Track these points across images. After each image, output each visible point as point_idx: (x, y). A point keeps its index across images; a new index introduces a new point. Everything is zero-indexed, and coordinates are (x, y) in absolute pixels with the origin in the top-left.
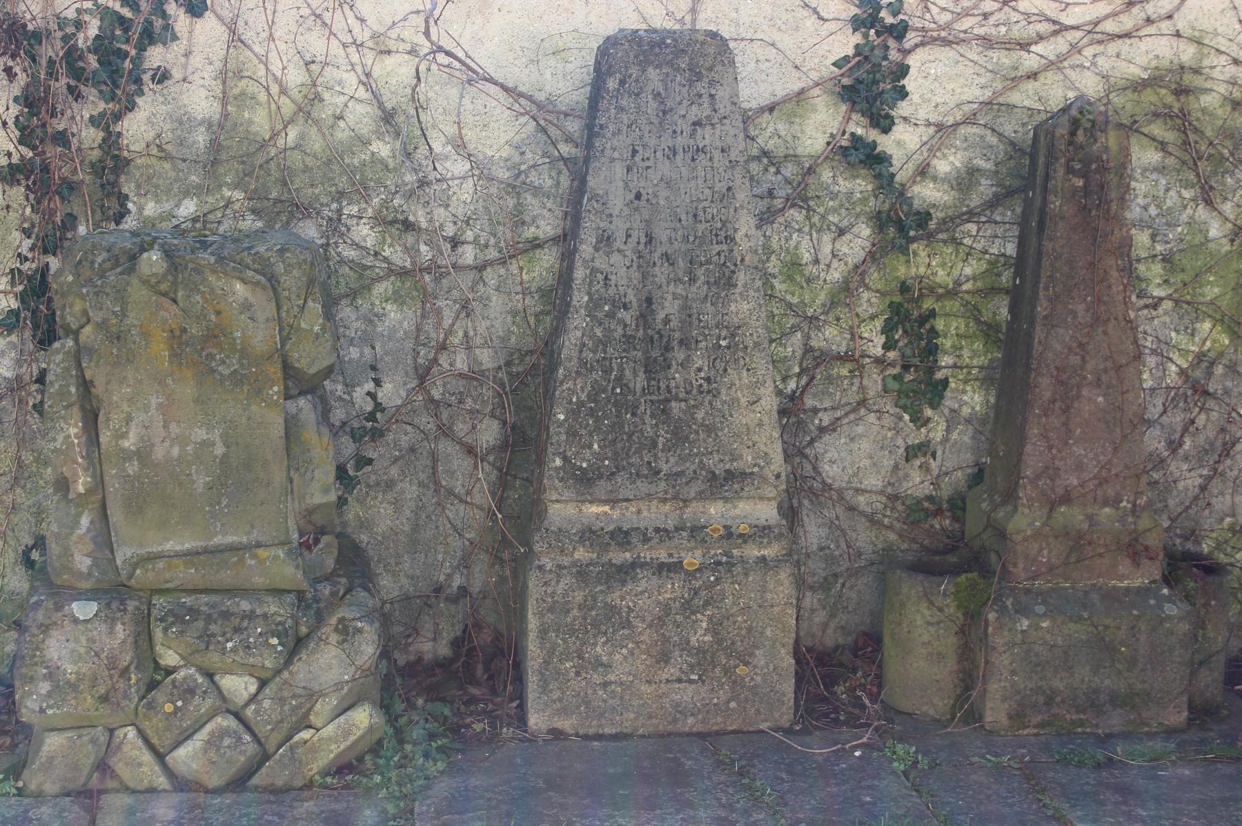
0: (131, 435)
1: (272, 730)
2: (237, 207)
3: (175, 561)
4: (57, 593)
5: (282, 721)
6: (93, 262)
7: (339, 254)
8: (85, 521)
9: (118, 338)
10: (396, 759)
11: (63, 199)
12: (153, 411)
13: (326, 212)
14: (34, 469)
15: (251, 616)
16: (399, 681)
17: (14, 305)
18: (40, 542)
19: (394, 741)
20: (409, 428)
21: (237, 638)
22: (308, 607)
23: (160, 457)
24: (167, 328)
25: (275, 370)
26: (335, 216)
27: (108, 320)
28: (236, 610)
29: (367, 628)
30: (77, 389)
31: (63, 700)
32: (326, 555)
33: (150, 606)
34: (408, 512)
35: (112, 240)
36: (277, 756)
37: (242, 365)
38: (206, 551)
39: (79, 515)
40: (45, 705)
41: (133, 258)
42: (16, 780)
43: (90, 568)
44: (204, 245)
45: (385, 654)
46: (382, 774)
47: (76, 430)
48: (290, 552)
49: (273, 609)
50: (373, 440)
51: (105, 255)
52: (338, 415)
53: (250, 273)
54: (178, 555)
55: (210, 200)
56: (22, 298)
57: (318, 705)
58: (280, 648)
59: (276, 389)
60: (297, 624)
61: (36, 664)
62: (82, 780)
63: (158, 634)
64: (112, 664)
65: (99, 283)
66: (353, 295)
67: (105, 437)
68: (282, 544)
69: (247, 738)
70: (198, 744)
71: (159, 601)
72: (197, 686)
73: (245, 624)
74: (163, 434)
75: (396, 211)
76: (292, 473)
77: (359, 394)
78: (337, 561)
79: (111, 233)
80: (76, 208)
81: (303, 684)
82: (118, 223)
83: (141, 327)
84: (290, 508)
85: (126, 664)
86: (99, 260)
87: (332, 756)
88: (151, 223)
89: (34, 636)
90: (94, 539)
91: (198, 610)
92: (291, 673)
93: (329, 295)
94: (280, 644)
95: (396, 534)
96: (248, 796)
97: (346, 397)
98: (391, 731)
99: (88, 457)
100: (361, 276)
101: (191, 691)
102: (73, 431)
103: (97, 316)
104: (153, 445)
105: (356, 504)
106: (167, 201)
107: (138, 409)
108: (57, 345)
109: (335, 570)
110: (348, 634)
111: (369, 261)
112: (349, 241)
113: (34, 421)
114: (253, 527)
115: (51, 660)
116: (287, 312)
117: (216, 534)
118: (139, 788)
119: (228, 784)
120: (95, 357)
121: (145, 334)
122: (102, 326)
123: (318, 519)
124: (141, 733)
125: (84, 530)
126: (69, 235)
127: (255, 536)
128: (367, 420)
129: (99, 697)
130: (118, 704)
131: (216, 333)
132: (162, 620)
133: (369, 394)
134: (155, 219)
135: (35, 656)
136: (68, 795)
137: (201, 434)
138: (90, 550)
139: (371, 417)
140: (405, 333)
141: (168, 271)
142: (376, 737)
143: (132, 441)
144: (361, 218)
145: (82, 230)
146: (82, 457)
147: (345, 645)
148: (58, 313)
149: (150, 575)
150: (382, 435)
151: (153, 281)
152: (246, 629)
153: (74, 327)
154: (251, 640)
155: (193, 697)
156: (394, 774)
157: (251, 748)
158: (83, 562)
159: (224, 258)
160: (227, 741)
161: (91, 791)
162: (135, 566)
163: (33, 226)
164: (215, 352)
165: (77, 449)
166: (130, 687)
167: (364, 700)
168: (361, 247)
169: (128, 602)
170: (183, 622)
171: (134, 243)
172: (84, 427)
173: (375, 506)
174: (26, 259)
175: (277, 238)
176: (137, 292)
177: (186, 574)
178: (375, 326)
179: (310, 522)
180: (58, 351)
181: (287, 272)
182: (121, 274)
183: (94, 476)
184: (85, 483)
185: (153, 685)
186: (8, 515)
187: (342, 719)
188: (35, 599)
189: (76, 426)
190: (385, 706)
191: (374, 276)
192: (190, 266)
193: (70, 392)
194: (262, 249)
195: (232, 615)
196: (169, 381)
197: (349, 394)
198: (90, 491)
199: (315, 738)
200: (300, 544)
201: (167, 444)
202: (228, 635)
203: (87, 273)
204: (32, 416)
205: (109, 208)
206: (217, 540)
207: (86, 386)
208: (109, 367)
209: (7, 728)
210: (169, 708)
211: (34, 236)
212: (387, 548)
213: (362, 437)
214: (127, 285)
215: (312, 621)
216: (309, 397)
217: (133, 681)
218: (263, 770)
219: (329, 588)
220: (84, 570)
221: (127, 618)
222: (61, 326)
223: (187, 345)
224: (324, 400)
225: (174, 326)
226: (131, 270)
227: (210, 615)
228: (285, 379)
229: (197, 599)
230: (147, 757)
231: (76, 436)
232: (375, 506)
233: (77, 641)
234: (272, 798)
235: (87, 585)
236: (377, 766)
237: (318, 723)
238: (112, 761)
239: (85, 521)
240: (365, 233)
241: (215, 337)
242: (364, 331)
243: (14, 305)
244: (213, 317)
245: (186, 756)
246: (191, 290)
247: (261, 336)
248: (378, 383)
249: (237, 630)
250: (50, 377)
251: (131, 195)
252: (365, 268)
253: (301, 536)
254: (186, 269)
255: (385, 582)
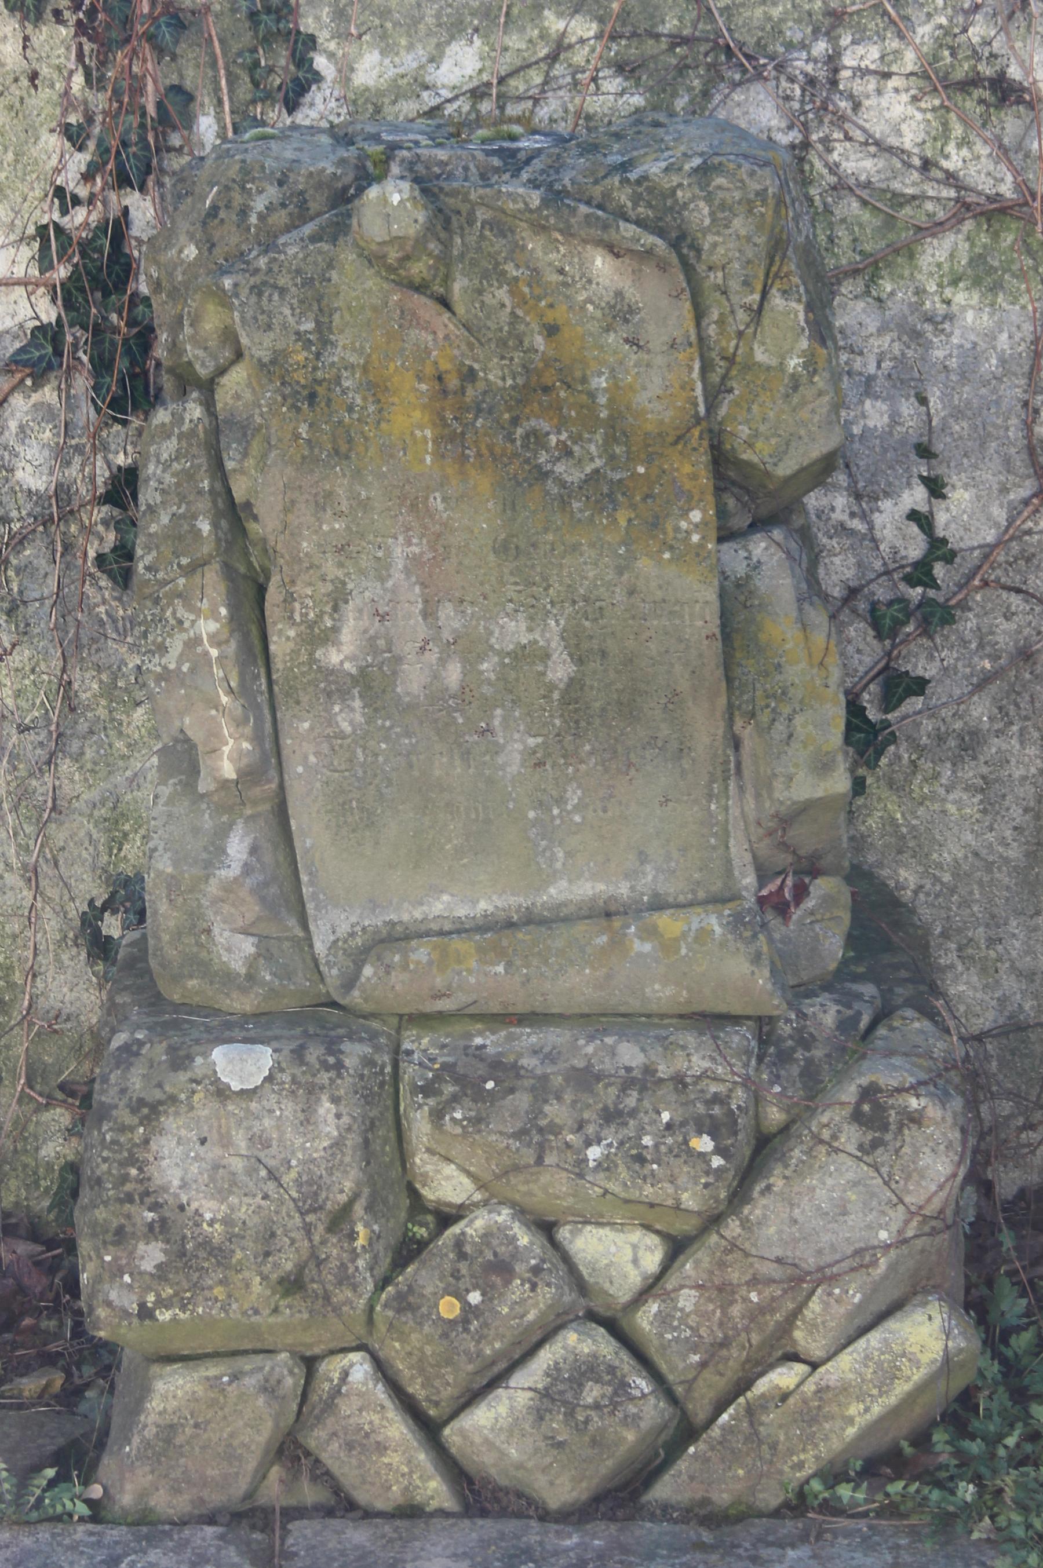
0: (346, 635)
1: (703, 1365)
2: (579, 57)
3: (457, 944)
4: (175, 1025)
5: (725, 1344)
6: (244, 212)
7: (833, 168)
8: (237, 847)
9: (312, 397)
10: (1011, 1441)
11: (160, 51)
12: (397, 575)
13: (800, 64)
14: (102, 712)
15: (644, 1081)
16: (1007, 1240)
17: (48, 312)
18: (127, 895)
19: (1002, 1396)
20: (1015, 601)
21: (610, 1137)
22: (784, 1057)
23: (415, 688)
24: (429, 370)
25: (692, 468)
26: (822, 74)
27: (285, 354)
28: (608, 1066)
29: (934, 1112)
30: (215, 525)
31: (195, 1286)
32: (824, 924)
33: (397, 1053)
34: (1016, 812)
35: (289, 154)
36: (715, 1432)
37: (612, 458)
38: (531, 919)
39: (223, 833)
40: (151, 1298)
41: (343, 198)
42: (86, 1483)
43: (252, 963)
44: (513, 162)
45: (978, 1180)
46: (977, 1479)
47: (213, 626)
48: (737, 922)
49: (699, 1063)
50: (926, 630)
51: (273, 192)
52: (839, 569)
53: (628, 230)
54: (461, 929)
55: (515, 41)
56: (69, 296)
57: (815, 1305)
58: (717, 1162)
59: (696, 516)
60: (757, 1099)
61: (129, 1198)
62: (242, 1486)
63: (420, 1126)
64: (310, 1201)
65: (262, 262)
66: (870, 269)
67: (282, 642)
68: (716, 900)
69: (642, 1384)
70: (523, 1398)
71: (419, 1043)
72: (516, 1254)
73: (631, 1100)
74: (422, 631)
75: (976, 55)
76: (739, 723)
77: (889, 517)
78: (851, 940)
79: (283, 136)
80: (190, 72)
81: (778, 1252)
82: (292, 107)
83: (365, 369)
84: (734, 812)
85: (343, 1198)
86: (259, 204)
87: (851, 1431)
88: (369, 104)
89: (123, 1129)
90: (257, 891)
91: (515, 1067)
92: (745, 1223)
93: (819, 277)
94: (718, 1151)
95: (989, 867)
96: (647, 1530)
97: (857, 524)
98: (994, 1369)
99: (244, 692)
100: (890, 221)
101: (501, 1269)
102: (207, 627)
103: (258, 345)
104: (398, 660)
105: (885, 793)
106: (410, 47)
107: (362, 572)
108: (162, 416)
109: (845, 962)
110: (885, 1127)
111: (908, 184)
112: (858, 135)
113: (101, 594)
114: (643, 857)
115: (165, 1189)
116: (721, 322)
117: (552, 877)
118: (380, 1505)
119: (597, 1499)
120: (256, 447)
121: (377, 389)
122: (272, 368)
123: (806, 837)
124: (382, 1368)
125: (234, 870)
126: (175, 140)
127: (649, 880)
128: (911, 581)
129: (281, 1281)
130: (327, 1297)
131: (548, 379)
132: (428, 1090)
133: (914, 516)
134: (380, 93)
135: (125, 1178)
136: (211, 1520)
137: (513, 631)
138: (250, 917)
139: (921, 573)
140: (1003, 361)
141: (429, 228)
142: (959, 1383)
143: (348, 649)
144: (887, 75)
145: (206, 126)
146: (231, 691)
147: (881, 1155)
148: (164, 337)
149: (398, 979)
150: (948, 618)
151: (393, 255)
152: (633, 1113)
153: (203, 372)
154: (647, 1141)
155: (507, 1283)
156: (1008, 1480)
157: (651, 1411)
158: (235, 950)
159: (563, 194)
160: (592, 1393)
161: (267, 1512)
162: (360, 957)
163: (90, 119)
164: (545, 426)
165: (218, 673)
166: (354, 1255)
167: (925, 1291)
168: (890, 150)
169: (347, 1046)
170: (480, 1095)
171: (342, 162)
172: (232, 618)
173: (933, 797)
174: (76, 201)
175: (691, 142)
176: (355, 285)
177: (481, 977)
178: (928, 346)
179: (784, 846)
180: (165, 432)
181: (720, 223)
182: (314, 238)
183: (257, 738)
184: (237, 756)
185: (407, 1252)
186: (42, 827)
187: (874, 1338)
188: (120, 1039)
189: (214, 615)
190: (976, 1306)
191: (922, 220)
192: (481, 214)
193: (197, 533)
194: (654, 168)
195: (598, 1078)
196: (436, 502)
197: (864, 517)
198: (249, 776)
199: (809, 1387)
200: (761, 901)
201: (432, 656)
202: (590, 1129)
203: (230, 238)
204: (95, 584)
205: (271, 70)
206: (558, 892)
207: (234, 515)
208: (289, 471)
209: (53, 1348)
210: (449, 1308)
211: (91, 145)
212: (966, 903)
213: (900, 623)
214: (330, 266)
215: (796, 1093)
216: (777, 534)
217: (360, 1242)
218: (682, 1465)
219: (833, 1009)
220: (238, 966)
221: (345, 1085)
222: (171, 371)
223: (479, 411)
224: (805, 536)
225: (445, 365)
226: (338, 230)
227: (545, 1078)
228: (718, 491)
229: (510, 1038)
230: (397, 1428)
231: (215, 640)
232: (933, 797)
233: (226, 1142)
234: (707, 1536)
235: (243, 1003)
236: (964, 1460)
237: (816, 1348)
238: (315, 1438)
239: (237, 847)
240: (897, 113)
241: (546, 389)
242: (900, 361)
243: (48, 312)
244: (540, 341)
245: (493, 1427)
246: (485, 275)
247: (657, 386)
248: (936, 488)
249: (611, 1116)
250: (148, 495)
251: (322, 36)
252: (899, 200)
253: (763, 879)
254: (471, 222)
255: (964, 987)
